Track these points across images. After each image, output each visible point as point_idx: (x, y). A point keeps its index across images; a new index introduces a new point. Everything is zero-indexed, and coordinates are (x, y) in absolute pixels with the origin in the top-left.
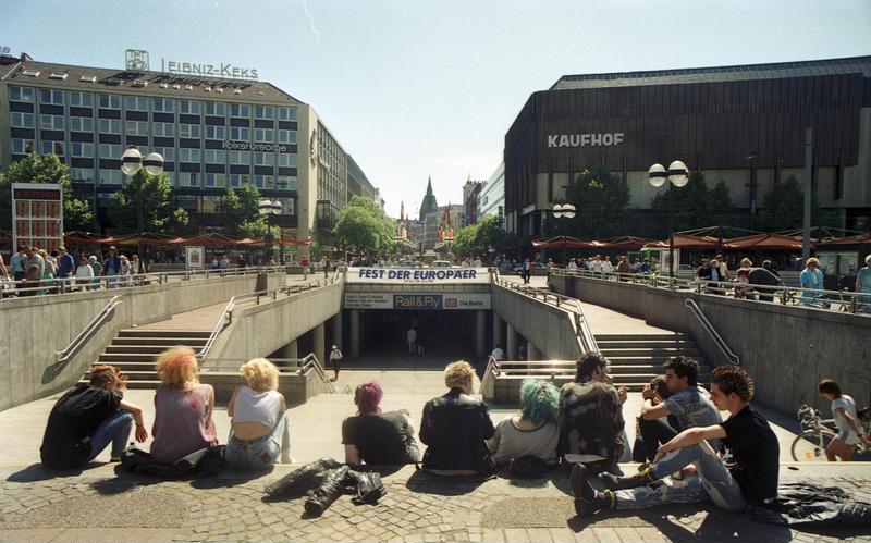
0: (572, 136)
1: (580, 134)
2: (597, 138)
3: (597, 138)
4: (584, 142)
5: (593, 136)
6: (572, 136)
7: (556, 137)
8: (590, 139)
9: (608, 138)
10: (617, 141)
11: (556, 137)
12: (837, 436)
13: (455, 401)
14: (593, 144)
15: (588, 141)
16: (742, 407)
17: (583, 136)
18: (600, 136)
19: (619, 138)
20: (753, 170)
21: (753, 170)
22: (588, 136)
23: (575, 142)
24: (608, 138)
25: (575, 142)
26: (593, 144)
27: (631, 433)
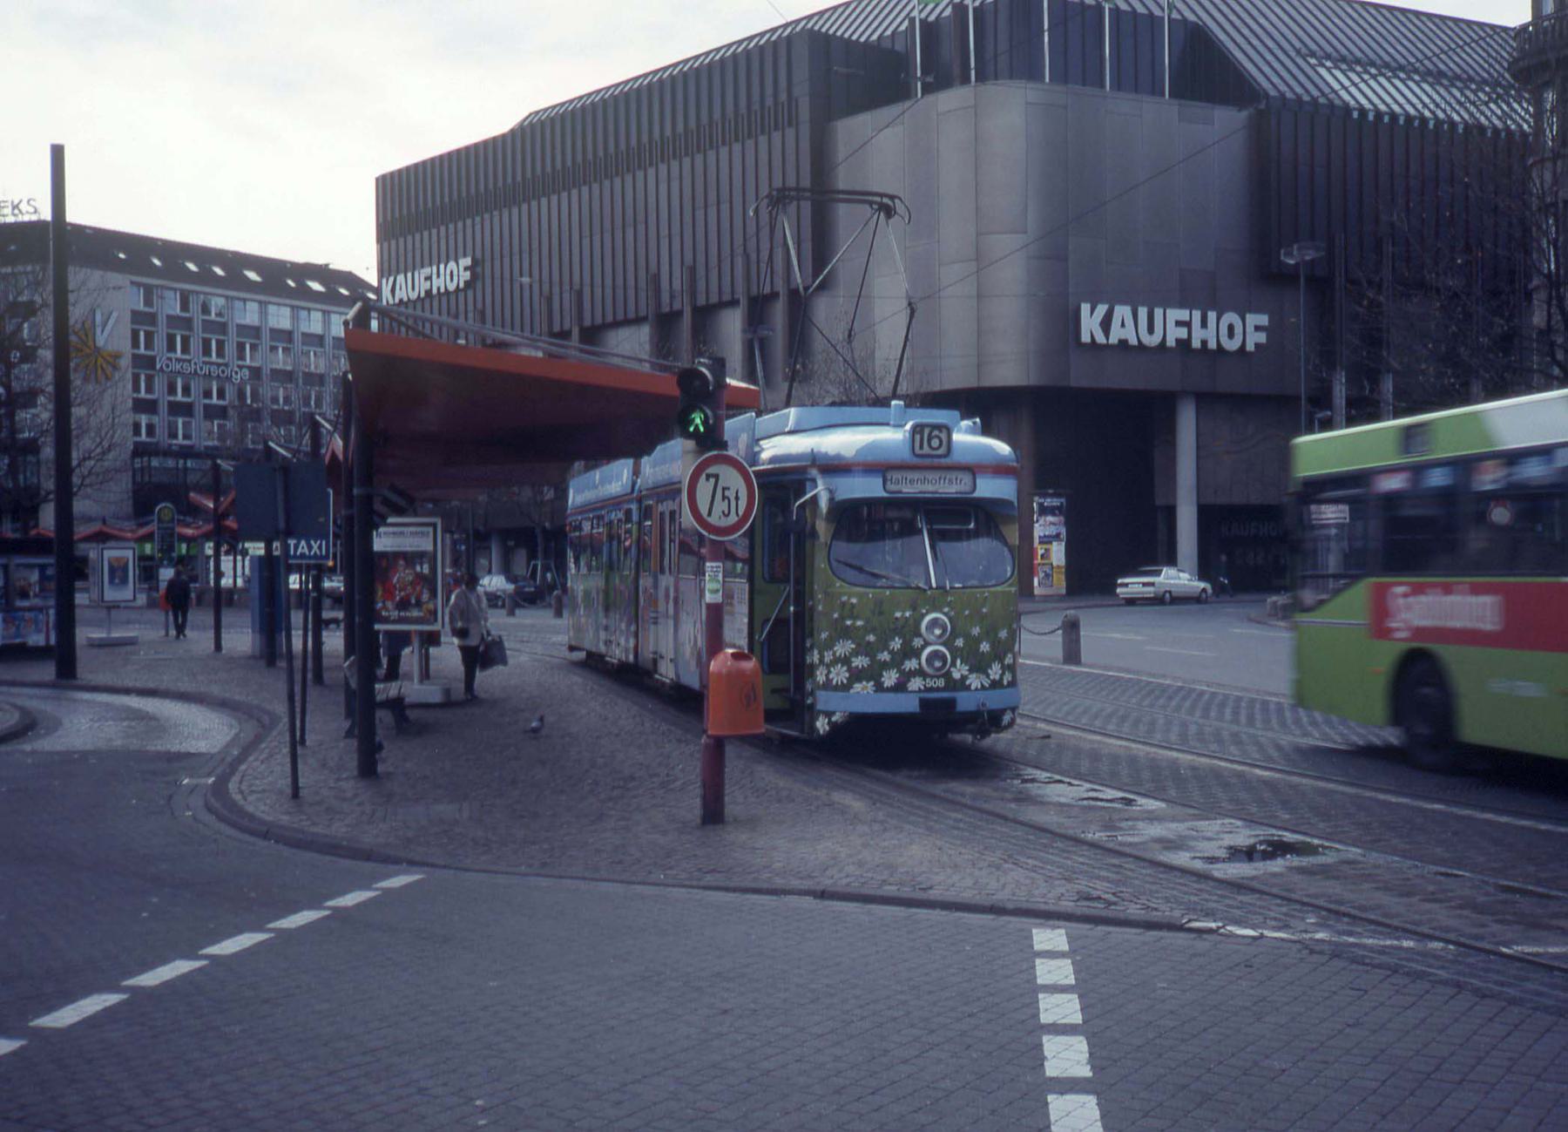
0: (1143, 312)
1: (1166, 305)
2: (1204, 324)
3: (1204, 324)
4: (1175, 334)
5: (1197, 315)
6: (1143, 312)
7: (1102, 309)
8: (1188, 324)
9: (1231, 328)
10: (1255, 339)
11: (1102, 309)
12: (416, 685)
13: (33, 532)
14: (1196, 344)
15: (1182, 333)
16: (341, 698)
17: (1176, 314)
18: (1212, 316)
19: (1257, 328)
20: (811, 190)
21: (811, 190)
22: (1183, 315)
23: (1151, 330)
24: (1231, 328)
25: (1151, 330)
26: (1196, 344)
27: (359, 305)
